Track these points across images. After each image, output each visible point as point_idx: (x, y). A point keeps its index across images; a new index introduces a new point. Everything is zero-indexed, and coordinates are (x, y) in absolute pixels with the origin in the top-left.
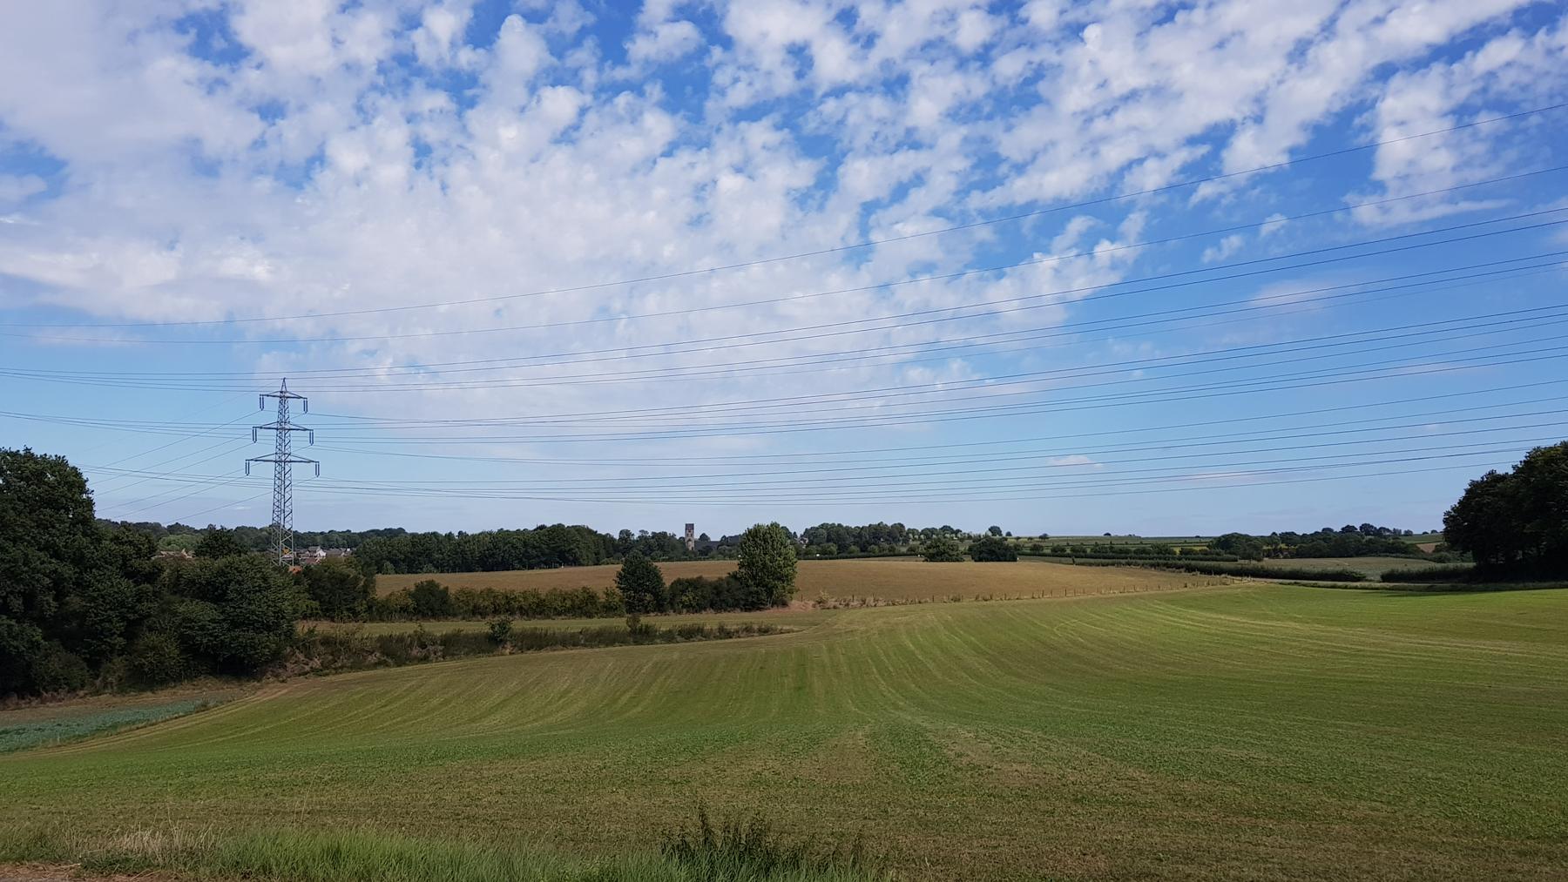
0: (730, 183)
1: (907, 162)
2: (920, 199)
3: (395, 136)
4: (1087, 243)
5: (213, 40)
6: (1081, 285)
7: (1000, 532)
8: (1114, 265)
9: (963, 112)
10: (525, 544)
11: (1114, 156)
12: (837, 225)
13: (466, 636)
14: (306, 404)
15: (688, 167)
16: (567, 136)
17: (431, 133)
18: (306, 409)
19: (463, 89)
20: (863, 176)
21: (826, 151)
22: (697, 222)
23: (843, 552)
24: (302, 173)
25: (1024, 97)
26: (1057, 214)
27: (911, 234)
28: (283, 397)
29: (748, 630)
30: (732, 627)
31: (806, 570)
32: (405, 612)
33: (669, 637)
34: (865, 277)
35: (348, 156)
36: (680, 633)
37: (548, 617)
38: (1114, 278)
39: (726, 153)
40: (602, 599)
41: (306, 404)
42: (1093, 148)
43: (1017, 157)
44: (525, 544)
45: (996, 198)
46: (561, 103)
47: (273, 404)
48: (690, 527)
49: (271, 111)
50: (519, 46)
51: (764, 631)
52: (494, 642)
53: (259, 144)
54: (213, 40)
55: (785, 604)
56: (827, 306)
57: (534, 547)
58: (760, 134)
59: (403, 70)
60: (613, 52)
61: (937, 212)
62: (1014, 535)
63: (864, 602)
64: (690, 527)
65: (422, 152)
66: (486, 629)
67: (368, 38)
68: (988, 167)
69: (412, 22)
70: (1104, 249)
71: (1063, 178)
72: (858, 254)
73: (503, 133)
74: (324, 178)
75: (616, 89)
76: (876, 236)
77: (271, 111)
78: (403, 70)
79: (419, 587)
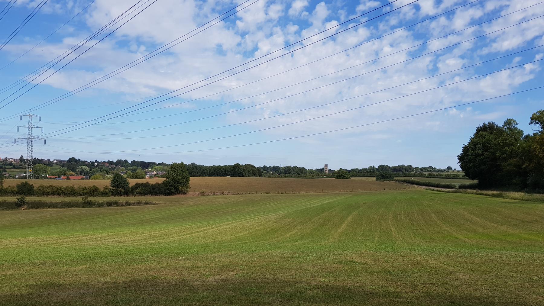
0: (387, 49)
1: (453, 39)
2: (456, 51)
3: (279, 39)
4: (521, 65)
5: (229, 15)
6: (518, 80)
7: (451, 169)
8: (532, 72)
9: (473, 22)
10: (226, 171)
11: (530, 35)
12: (425, 61)
13: (8, 203)
14: (40, 118)
15: (375, 45)
16: (332, 37)
17: (292, 39)
18: (40, 120)
19: (304, 24)
20: (435, 45)
21: (423, 37)
22: (374, 62)
23: (240, 175)
24: (250, 53)
25: (491, 17)
26: (509, 55)
27: (452, 63)
28: (30, 116)
29: (139, 203)
30: (132, 202)
31: (193, 180)
32: (13, 193)
33: (101, 205)
34: (435, 79)
35: (265, 47)
36: (107, 203)
37: (75, 196)
38: (532, 77)
39: (387, 39)
40: (102, 190)
41: (40, 118)
42: (523, 32)
43: (492, 36)
44: (226, 171)
45: (485, 51)
46: (333, 26)
47: (26, 120)
48: (326, 166)
49: (243, 34)
50: (322, 10)
51: (146, 204)
52: (19, 205)
53: (239, 44)
54: (229, 15)
55: (185, 193)
56: (420, 89)
57: (228, 172)
58: (400, 33)
59: (284, 21)
60: (351, 10)
61: (462, 57)
62: (329, 168)
63: (223, 193)
64: (326, 166)
65: (288, 45)
66: (16, 200)
67: (275, 11)
68: (481, 40)
69: (289, 6)
70: (528, 67)
71: (509, 44)
72: (434, 71)
73: (312, 36)
74: (257, 54)
75: (349, 21)
76: (440, 65)
77: (243, 34)
78: (284, 21)
79: (22, 184)
